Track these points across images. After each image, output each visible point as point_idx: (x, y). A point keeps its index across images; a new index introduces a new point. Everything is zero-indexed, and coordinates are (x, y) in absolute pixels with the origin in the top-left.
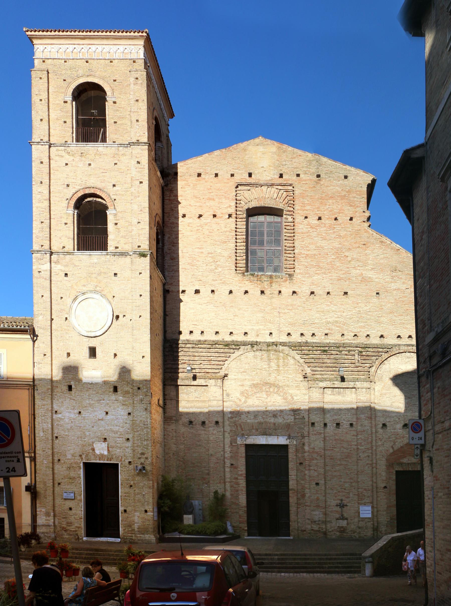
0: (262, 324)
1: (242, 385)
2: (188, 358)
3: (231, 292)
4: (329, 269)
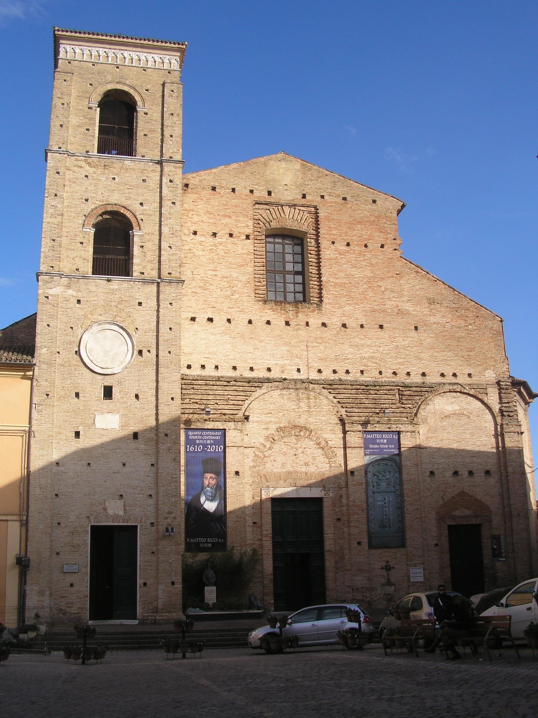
0: (288, 358)
1: (267, 429)
2: (199, 397)
3: (250, 322)
4: (361, 300)
